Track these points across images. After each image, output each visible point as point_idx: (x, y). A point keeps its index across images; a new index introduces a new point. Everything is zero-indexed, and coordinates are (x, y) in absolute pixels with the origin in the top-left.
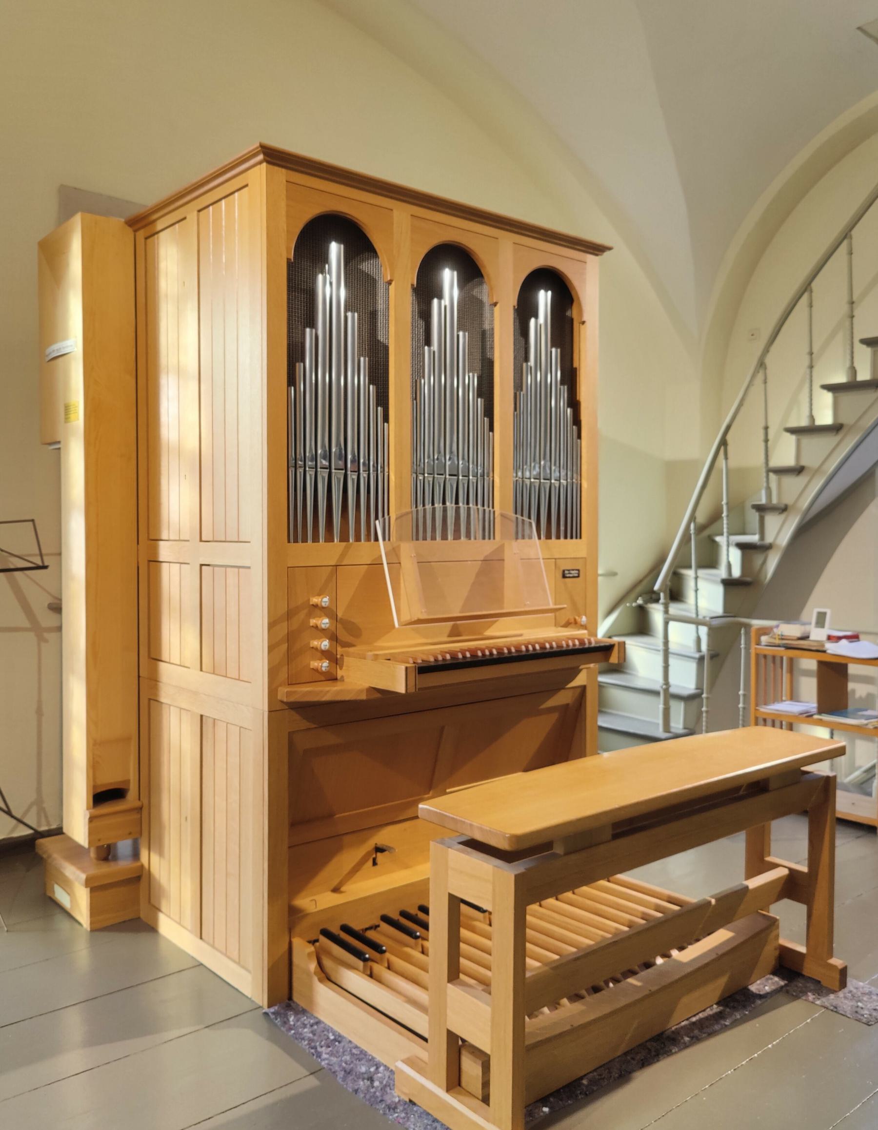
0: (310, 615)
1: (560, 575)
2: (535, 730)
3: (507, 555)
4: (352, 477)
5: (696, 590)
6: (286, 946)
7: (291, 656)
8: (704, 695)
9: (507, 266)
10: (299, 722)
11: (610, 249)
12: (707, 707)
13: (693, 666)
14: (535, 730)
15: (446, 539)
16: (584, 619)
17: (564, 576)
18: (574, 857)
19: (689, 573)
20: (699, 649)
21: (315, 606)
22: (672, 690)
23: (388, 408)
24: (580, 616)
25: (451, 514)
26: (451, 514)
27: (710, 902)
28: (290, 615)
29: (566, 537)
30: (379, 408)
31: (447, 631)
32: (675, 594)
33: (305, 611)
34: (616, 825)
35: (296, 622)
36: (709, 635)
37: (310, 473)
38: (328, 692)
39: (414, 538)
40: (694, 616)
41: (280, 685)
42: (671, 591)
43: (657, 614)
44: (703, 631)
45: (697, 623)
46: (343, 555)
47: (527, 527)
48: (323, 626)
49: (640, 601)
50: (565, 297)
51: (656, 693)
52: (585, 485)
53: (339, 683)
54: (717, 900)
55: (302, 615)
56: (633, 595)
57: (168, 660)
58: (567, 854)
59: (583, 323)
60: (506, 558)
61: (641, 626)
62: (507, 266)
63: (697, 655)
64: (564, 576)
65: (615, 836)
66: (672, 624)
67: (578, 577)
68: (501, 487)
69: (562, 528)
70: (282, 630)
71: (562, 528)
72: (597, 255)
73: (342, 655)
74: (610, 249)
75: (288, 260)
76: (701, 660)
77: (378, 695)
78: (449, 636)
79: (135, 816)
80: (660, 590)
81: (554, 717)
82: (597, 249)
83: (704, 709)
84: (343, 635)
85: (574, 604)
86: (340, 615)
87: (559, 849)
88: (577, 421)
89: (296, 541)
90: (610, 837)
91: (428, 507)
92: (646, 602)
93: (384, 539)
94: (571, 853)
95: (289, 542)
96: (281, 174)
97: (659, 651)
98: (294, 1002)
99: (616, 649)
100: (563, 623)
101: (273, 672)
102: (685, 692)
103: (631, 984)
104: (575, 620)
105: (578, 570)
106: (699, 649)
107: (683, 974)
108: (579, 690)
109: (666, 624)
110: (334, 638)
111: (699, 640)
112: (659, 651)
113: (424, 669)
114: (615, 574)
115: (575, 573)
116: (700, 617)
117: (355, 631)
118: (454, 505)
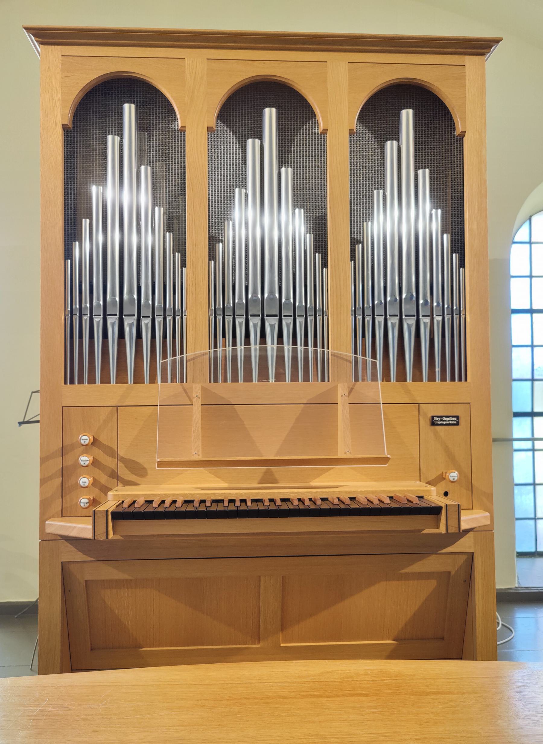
1: (425, 423)
2: (395, 599)
4: (425, 321)
7: (63, 491)
11: (497, 41)
14: (395, 599)
15: (237, 381)
17: (433, 424)
25: (300, 356)
26: (300, 356)
29: (453, 379)
30: (445, 236)
35: (69, 460)
37: (379, 320)
60: (339, 403)
64: (433, 424)
67: (457, 424)
69: (438, 369)
70: (56, 465)
71: (438, 369)
72: (483, 54)
74: (497, 41)
75: (64, 127)
78: (260, 482)
82: (480, 47)
84: (124, 473)
86: (121, 453)
88: (458, 246)
89: (72, 382)
91: (255, 347)
95: (65, 383)
96: (56, 51)
100: (432, 476)
105: (457, 417)
115: (452, 420)
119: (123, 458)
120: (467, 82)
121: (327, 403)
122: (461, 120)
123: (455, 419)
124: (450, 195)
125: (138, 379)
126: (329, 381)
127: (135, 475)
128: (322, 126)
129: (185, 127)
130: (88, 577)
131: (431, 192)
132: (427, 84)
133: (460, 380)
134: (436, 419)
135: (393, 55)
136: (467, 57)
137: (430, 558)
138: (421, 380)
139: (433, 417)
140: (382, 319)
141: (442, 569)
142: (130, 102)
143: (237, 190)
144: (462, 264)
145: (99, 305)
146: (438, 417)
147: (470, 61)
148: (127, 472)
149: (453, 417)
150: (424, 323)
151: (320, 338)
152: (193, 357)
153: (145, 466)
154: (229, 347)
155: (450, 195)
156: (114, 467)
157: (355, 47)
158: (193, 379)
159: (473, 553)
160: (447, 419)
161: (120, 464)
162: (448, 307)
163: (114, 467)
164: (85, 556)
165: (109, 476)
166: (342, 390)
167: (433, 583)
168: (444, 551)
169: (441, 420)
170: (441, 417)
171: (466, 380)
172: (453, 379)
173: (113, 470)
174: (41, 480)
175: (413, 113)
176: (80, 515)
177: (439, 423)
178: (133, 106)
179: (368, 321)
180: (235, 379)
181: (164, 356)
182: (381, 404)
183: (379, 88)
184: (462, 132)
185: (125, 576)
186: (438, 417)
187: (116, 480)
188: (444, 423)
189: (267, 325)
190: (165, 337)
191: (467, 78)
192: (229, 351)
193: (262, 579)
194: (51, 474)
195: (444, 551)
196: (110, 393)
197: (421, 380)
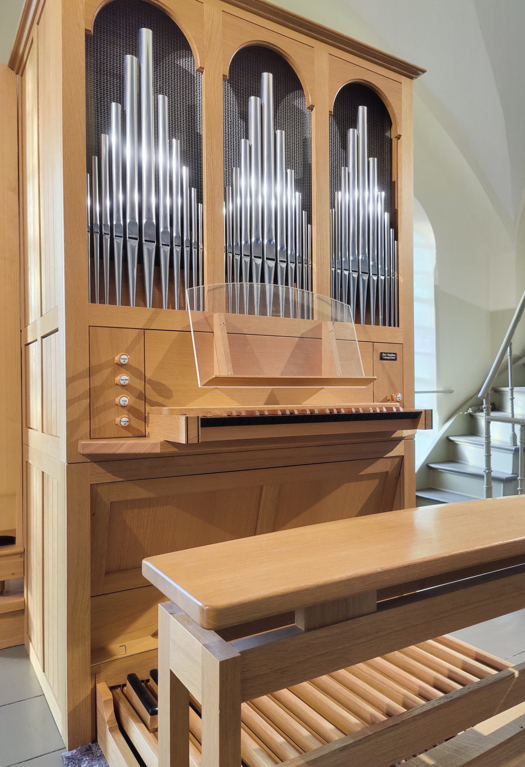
0: (115, 373)
1: (377, 357)
3: (324, 334)
5: (512, 399)
6: (89, 692)
7: (91, 412)
8: (519, 478)
9: (323, 77)
10: (101, 475)
12: (521, 487)
13: (510, 457)
16: (400, 395)
17: (382, 358)
18: (320, 633)
19: (508, 389)
20: (515, 444)
21: (121, 365)
22: (493, 474)
23: (202, 189)
24: (396, 392)
27: (513, 674)
28: (91, 372)
29: (390, 325)
31: (265, 397)
32: (496, 406)
33: (109, 370)
34: (382, 592)
35: (98, 380)
36: (522, 431)
38: (123, 444)
39: (230, 310)
40: (510, 415)
41: (82, 439)
42: (493, 404)
43: (482, 418)
44: (518, 427)
45: (513, 421)
46: (151, 320)
47: (345, 311)
48: (122, 382)
49: (470, 411)
50: (382, 120)
51: (481, 477)
52: (401, 280)
53: (147, 438)
54: (521, 672)
55: (107, 372)
56: (465, 407)
57: (35, 428)
58: (308, 630)
59: (399, 137)
60: (323, 338)
61: (472, 429)
62: (323, 77)
63: (513, 448)
64: (382, 358)
65: (381, 607)
66: (492, 423)
67: (396, 360)
68: (318, 273)
69: (381, 317)
70: (83, 385)
71: (381, 317)
72: (412, 78)
73: (148, 413)
76: (516, 451)
77: (173, 449)
79: (19, 560)
80: (483, 397)
81: (375, 483)
83: (519, 488)
84: (151, 394)
85: (392, 385)
86: (148, 375)
87: (300, 624)
88: (394, 224)
90: (374, 607)
92: (475, 411)
93: (192, 308)
94: (315, 629)
97: (483, 445)
98: (97, 745)
99: (423, 415)
101: (72, 427)
102: (504, 476)
103: (423, 762)
104: (392, 396)
105: (396, 354)
106: (515, 444)
107: (482, 751)
108: (397, 460)
109: (488, 423)
110: (142, 397)
111: (514, 436)
112: (483, 445)
113: (208, 422)
114: (451, 392)
116: (515, 417)
117: (165, 392)
118: (273, 285)
119: (149, 380)
120: (403, 96)
121: (205, 333)
122: (311, 95)
123: (394, 355)
124: (388, 182)
125: (157, 304)
126: (204, 310)
127: (162, 396)
128: (198, 64)
129: (203, 68)
130: (115, 499)
131: (378, 176)
132: (287, 56)
133: (308, 318)
134: (384, 355)
135: (302, 35)
136: (403, 77)
137: (379, 461)
138: (379, 325)
139: (381, 353)
140: (136, 243)
141: (384, 469)
142: (363, 105)
143: (343, 168)
144: (200, 199)
145: (118, 224)
146: (385, 353)
147: (404, 80)
148: (154, 393)
149: (394, 354)
150: (281, 267)
151: (305, 283)
152: (212, 288)
153: (170, 388)
154: (237, 282)
155: (388, 182)
156: (141, 388)
157: (334, 43)
158: (213, 309)
159: (403, 456)
160: (390, 355)
161: (147, 386)
162: (299, 256)
163: (141, 388)
164: (114, 477)
165: (138, 398)
166: (219, 322)
167: (376, 482)
168: (387, 456)
169: (387, 356)
170: (387, 353)
171: (313, 319)
172: (384, 324)
173: (141, 392)
174: (67, 401)
175: (368, 110)
176: (108, 437)
177: (385, 358)
178: (271, 75)
179: (106, 240)
180: (251, 311)
181: (191, 285)
182: (192, 332)
183: (245, 45)
184: (312, 105)
185: (151, 495)
186: (385, 353)
187: (144, 402)
188: (388, 358)
189: (266, 267)
190: (182, 267)
191: (403, 94)
192: (238, 287)
193: (265, 488)
194: (78, 395)
195: (387, 456)
196: (135, 316)
197: (379, 325)
